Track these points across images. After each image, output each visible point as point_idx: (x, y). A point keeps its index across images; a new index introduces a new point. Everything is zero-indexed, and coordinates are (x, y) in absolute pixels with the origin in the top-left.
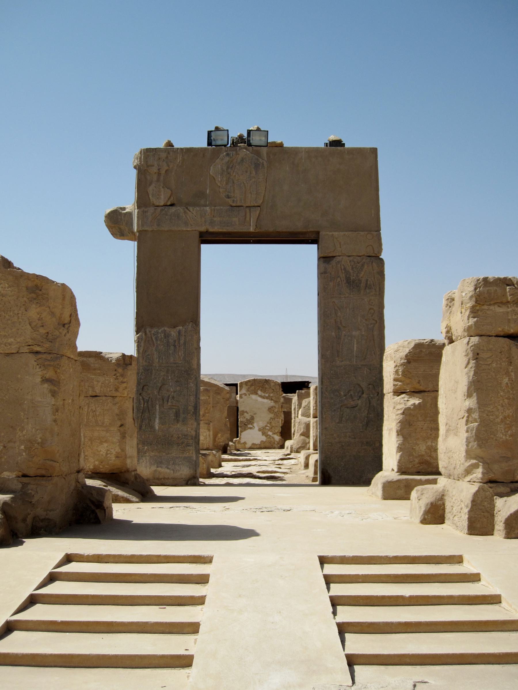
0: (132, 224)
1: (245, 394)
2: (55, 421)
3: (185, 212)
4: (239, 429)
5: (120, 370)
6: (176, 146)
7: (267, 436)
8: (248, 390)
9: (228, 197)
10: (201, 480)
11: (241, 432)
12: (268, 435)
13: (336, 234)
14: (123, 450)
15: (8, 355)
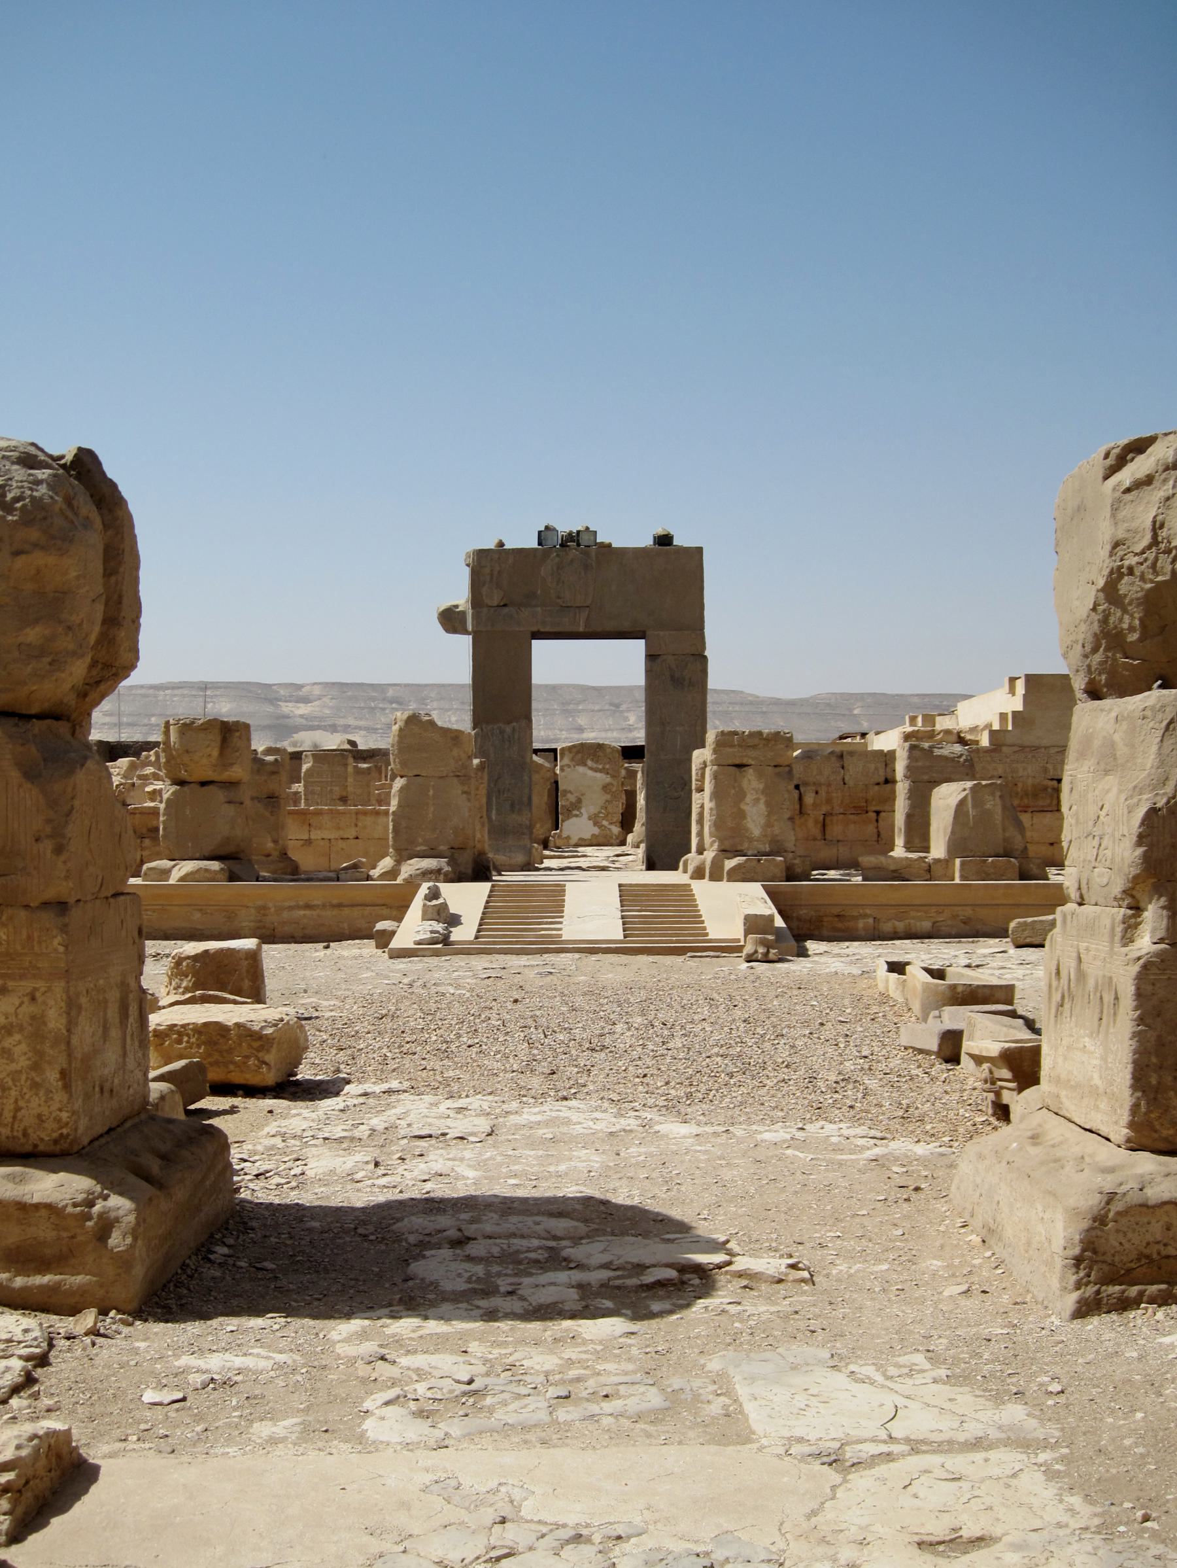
0: (465, 623)
1: (569, 766)
4: (560, 817)
5: (480, 774)
6: (507, 547)
7: (600, 827)
8: (572, 760)
9: (559, 598)
11: (563, 821)
12: (602, 826)
13: (662, 633)
15: (441, 777)
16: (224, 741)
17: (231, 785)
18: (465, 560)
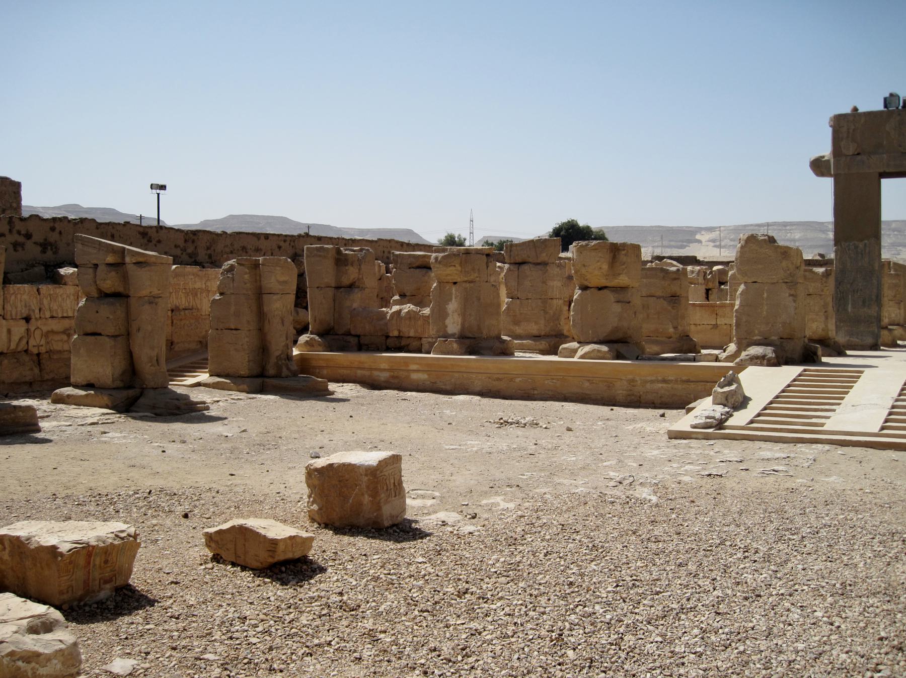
2: (795, 314)
3: (868, 159)
5: (824, 279)
9: (900, 146)
10: (882, 348)
14: (826, 326)
15: (773, 283)
16: (614, 258)
17: (621, 289)
18: (829, 123)
